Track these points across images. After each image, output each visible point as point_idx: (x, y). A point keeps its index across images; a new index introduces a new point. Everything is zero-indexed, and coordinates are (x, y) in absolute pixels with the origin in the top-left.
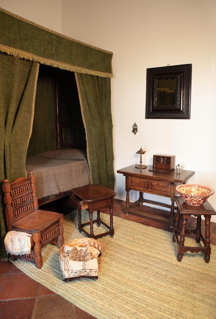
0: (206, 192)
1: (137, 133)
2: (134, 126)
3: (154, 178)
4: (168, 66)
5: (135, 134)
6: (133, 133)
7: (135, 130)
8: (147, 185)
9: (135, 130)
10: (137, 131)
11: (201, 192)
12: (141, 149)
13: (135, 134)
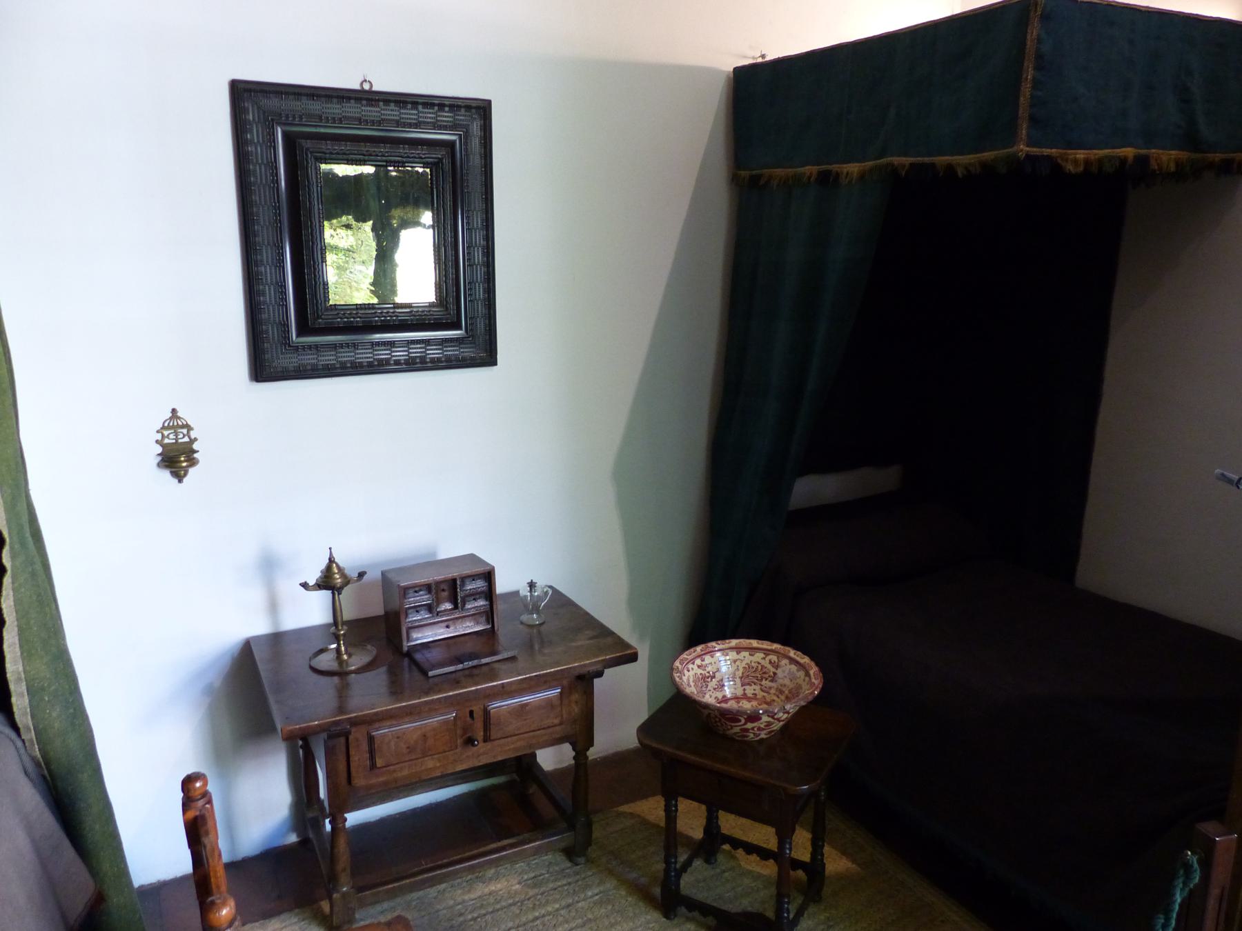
0: (763, 662)
1: (191, 471)
2: (163, 428)
3: (514, 687)
4: (366, 87)
5: (179, 476)
6: (166, 474)
7: (176, 458)
8: (459, 732)
9: (176, 458)
10: (193, 462)
11: (741, 670)
12: (331, 560)
13: (179, 476)
